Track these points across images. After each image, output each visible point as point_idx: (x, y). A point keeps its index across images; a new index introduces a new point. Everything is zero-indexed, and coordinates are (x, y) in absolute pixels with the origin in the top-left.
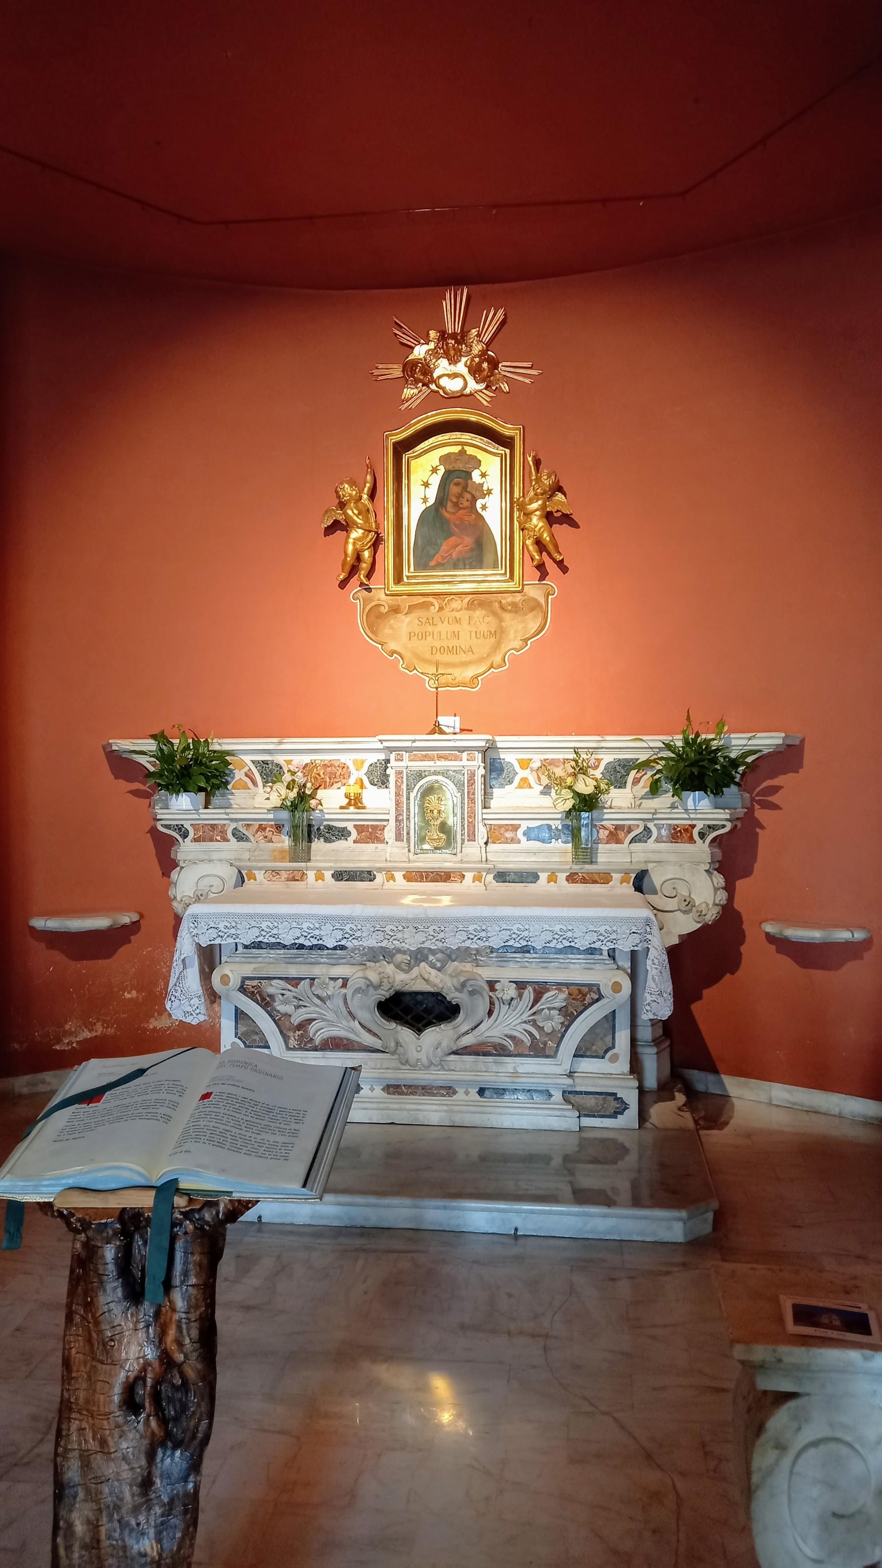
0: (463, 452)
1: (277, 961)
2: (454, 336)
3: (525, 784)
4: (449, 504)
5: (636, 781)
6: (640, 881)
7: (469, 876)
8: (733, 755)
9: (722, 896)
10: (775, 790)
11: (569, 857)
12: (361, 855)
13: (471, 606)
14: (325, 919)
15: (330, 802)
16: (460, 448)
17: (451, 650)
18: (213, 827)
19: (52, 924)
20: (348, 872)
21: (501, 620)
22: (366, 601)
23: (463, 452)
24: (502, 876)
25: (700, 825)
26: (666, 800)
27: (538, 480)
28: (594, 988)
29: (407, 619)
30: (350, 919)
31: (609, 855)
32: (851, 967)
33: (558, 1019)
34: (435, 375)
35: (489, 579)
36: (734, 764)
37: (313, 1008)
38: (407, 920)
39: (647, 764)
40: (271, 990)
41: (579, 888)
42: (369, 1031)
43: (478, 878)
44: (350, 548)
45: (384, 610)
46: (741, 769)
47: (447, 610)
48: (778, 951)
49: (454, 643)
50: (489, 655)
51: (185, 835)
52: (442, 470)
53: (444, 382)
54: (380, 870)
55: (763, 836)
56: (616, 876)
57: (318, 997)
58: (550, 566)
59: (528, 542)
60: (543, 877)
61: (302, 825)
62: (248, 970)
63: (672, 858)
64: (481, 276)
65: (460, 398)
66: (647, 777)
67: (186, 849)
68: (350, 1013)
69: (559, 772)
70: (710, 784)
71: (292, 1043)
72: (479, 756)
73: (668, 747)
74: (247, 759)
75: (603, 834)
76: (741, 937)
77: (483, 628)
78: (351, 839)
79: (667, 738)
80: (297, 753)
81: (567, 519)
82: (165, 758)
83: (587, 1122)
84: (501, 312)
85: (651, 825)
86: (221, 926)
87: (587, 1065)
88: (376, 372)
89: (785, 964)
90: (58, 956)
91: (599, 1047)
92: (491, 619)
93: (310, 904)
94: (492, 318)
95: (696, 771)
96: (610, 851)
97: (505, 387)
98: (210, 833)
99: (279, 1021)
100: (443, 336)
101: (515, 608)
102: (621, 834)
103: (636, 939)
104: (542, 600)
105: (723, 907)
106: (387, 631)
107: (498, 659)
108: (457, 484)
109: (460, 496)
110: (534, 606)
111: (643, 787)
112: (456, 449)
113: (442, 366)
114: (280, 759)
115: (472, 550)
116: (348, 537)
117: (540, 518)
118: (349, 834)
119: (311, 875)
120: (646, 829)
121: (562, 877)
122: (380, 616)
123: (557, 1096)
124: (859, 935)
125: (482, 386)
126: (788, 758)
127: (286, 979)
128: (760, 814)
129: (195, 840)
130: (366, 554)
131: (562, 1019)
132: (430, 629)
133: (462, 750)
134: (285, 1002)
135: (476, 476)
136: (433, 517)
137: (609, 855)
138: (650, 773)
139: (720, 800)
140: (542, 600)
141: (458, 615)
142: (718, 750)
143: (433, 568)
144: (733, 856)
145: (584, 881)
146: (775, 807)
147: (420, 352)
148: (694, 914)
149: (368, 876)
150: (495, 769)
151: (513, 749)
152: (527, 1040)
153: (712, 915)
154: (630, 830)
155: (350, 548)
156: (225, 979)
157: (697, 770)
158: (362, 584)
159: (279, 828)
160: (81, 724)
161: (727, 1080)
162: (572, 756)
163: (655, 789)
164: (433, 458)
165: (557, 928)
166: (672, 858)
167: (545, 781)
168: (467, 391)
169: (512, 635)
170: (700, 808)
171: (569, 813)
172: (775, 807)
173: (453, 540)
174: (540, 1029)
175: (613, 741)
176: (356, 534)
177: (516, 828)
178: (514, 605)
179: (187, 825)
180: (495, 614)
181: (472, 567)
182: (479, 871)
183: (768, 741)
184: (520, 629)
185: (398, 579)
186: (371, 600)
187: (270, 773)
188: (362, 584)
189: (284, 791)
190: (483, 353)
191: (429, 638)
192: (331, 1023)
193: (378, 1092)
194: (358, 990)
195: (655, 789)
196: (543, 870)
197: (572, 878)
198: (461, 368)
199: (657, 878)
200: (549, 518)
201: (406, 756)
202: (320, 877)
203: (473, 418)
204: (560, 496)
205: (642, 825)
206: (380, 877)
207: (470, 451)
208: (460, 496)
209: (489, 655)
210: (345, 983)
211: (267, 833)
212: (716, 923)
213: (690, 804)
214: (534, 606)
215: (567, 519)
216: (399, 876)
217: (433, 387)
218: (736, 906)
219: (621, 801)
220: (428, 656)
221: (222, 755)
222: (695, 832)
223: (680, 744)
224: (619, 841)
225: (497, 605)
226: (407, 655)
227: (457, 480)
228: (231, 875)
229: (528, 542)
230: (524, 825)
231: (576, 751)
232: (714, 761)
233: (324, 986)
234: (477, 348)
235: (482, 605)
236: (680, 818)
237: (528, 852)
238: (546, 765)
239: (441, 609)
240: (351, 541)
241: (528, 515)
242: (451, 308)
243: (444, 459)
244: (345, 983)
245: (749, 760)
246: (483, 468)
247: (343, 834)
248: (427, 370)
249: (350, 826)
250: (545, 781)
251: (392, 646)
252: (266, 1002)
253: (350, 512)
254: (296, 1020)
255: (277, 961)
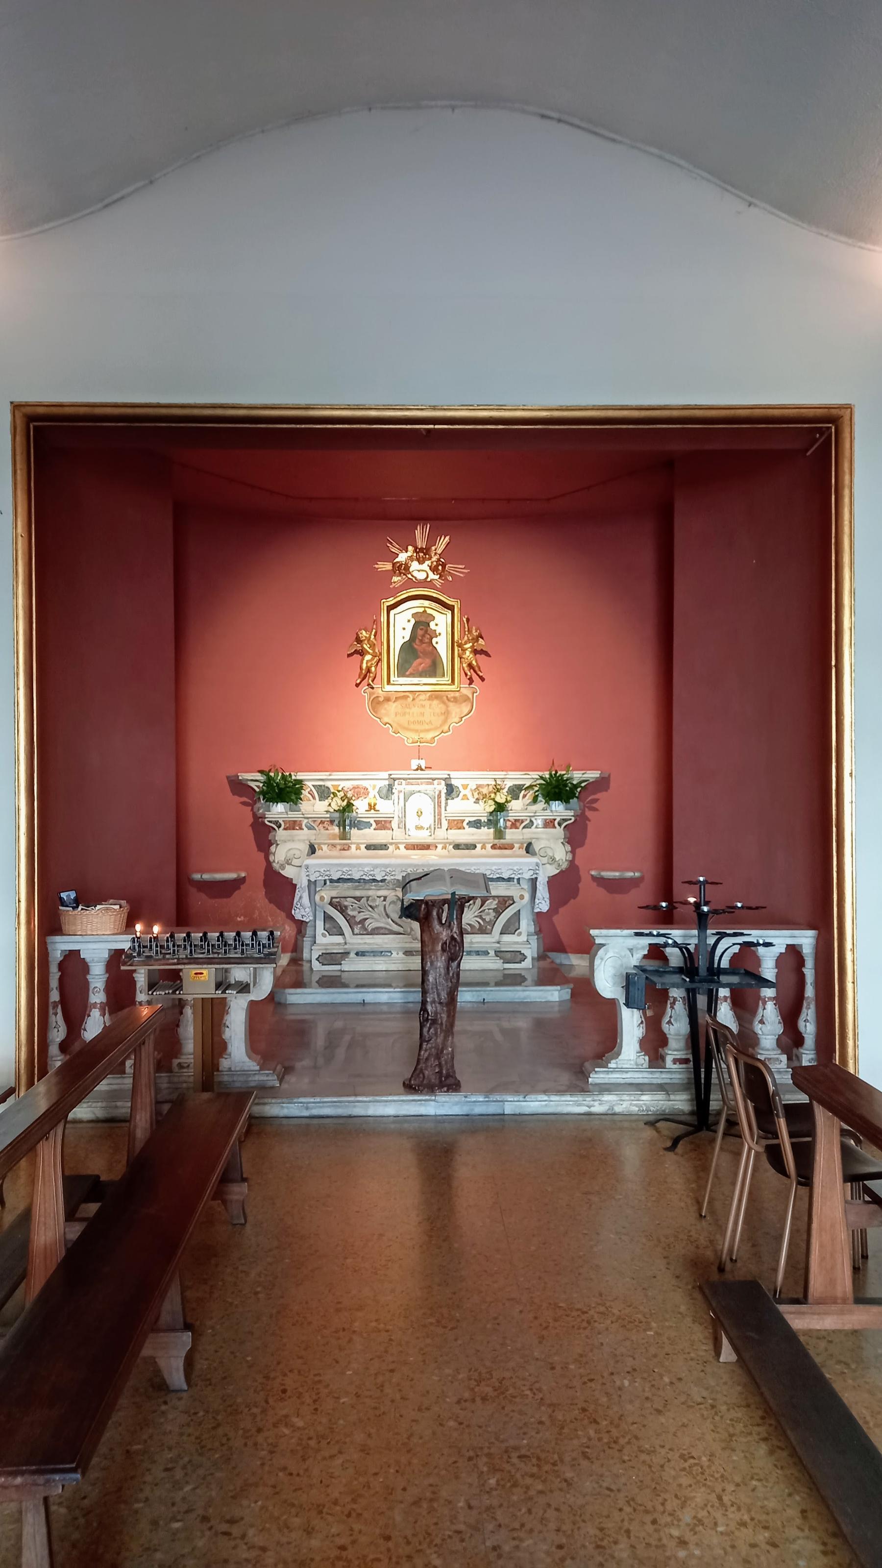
0: (425, 611)
1: (348, 888)
2: (421, 550)
3: (465, 797)
4: (417, 641)
5: (524, 796)
6: (529, 849)
7: (440, 846)
8: (575, 782)
9: (570, 857)
10: (596, 800)
11: (492, 836)
12: (381, 836)
13: (430, 698)
14: (376, 866)
15: (360, 806)
16: (422, 609)
17: (419, 722)
18: (295, 822)
19: (206, 877)
20: (374, 845)
21: (447, 707)
22: (371, 694)
23: (425, 611)
24: (457, 847)
25: (558, 819)
26: (541, 805)
27: (470, 631)
28: (511, 898)
29: (395, 705)
30: (387, 866)
31: (511, 835)
32: (634, 892)
33: (493, 914)
34: (411, 570)
35: (440, 683)
36: (575, 786)
37: (368, 913)
38: (418, 865)
39: (531, 787)
40: (346, 903)
41: (498, 852)
42: (396, 924)
43: (444, 848)
44: (364, 666)
45: (381, 699)
46: (579, 790)
47: (417, 700)
48: (598, 885)
49: (421, 719)
50: (441, 726)
51: (279, 827)
52: (413, 621)
53: (415, 574)
54: (392, 844)
55: (590, 827)
56: (517, 846)
57: (371, 906)
58: (475, 677)
59: (464, 665)
60: (479, 846)
61: (345, 819)
62: (334, 893)
63: (544, 836)
64: (439, 517)
65: (425, 583)
66: (531, 794)
67: (281, 834)
68: (387, 915)
69: (485, 791)
70: (565, 797)
71: (356, 931)
72: (443, 782)
73: (542, 778)
74: (310, 784)
75: (509, 824)
76: (579, 879)
77: (438, 711)
78: (372, 828)
79: (541, 773)
80: (342, 781)
81: (482, 652)
82: (269, 782)
83: (507, 966)
84: (447, 538)
85: (533, 819)
86: (322, 870)
87: (507, 938)
88: (376, 566)
89: (601, 892)
90: (203, 896)
91: (512, 929)
92: (442, 705)
93: (357, 860)
94: (443, 542)
95: (557, 790)
96: (513, 833)
97: (450, 579)
98: (293, 825)
99: (351, 921)
100: (416, 550)
101: (455, 700)
102: (518, 824)
103: (531, 872)
104: (471, 696)
105: (570, 861)
106: (383, 711)
107: (446, 728)
108: (422, 629)
109: (423, 636)
110: (466, 699)
111: (529, 798)
112: (421, 610)
113: (415, 566)
114: (329, 784)
115: (430, 666)
116: (363, 659)
117: (471, 652)
118: (371, 825)
119: (353, 847)
120: (531, 821)
121: (489, 846)
122: (379, 703)
123: (492, 953)
124: (637, 874)
125: (437, 577)
126: (602, 784)
127: (354, 898)
128: (588, 813)
129: (285, 829)
130: (373, 669)
131: (494, 914)
132: (407, 710)
133: (434, 779)
134: (353, 910)
135: (432, 625)
136: (408, 648)
137: (511, 835)
138: (531, 792)
139: (568, 806)
140: (471, 696)
141: (424, 703)
142: (567, 780)
143: (408, 676)
144: (575, 834)
145: (500, 848)
146: (596, 810)
147: (402, 557)
148: (555, 865)
149: (384, 847)
150: (451, 790)
151: (459, 778)
152: (477, 925)
153: (565, 866)
154: (522, 822)
155: (364, 666)
156: (322, 898)
157: (556, 790)
158: (369, 685)
159: (332, 822)
160: (218, 761)
161: (572, 956)
162: (494, 783)
163: (535, 800)
164: (408, 615)
165: (493, 868)
166: (544, 836)
167: (476, 796)
168: (429, 580)
169: (453, 715)
170: (558, 809)
171: (491, 813)
172: (596, 810)
173: (419, 660)
174: (484, 920)
175: (512, 774)
176: (368, 657)
177: (463, 821)
178: (455, 698)
179: (281, 821)
180: (444, 703)
181: (430, 676)
182: (445, 844)
183: (593, 775)
184: (458, 711)
185: (389, 682)
186: (374, 693)
187: (324, 793)
188: (369, 685)
189: (339, 802)
190: (439, 560)
191: (407, 716)
192: (377, 920)
193: (401, 955)
194: (393, 902)
195: (535, 800)
196: (479, 843)
197: (494, 847)
198: (425, 566)
199: (536, 847)
200: (475, 652)
201: (404, 782)
202: (358, 848)
203: (435, 595)
204: (481, 641)
205: (528, 819)
206: (391, 848)
207: (429, 611)
208: (423, 636)
209: (441, 726)
210: (385, 898)
211: (325, 825)
212: (567, 869)
213: (553, 808)
214: (466, 699)
215: (482, 652)
216: (402, 847)
217: (409, 576)
218: (577, 862)
219: (516, 807)
220: (406, 725)
221: (300, 782)
222: (556, 823)
223: (548, 776)
224: (517, 828)
225: (445, 698)
226: (394, 725)
227: (422, 625)
228: (306, 848)
229: (464, 665)
230: (467, 820)
231: (495, 780)
232: (566, 785)
233: (374, 900)
234: (434, 559)
235: (437, 697)
236: (549, 816)
237: (469, 834)
238: (479, 787)
239: (414, 699)
240: (365, 662)
241: (464, 650)
242: (421, 535)
243: (414, 615)
244: (385, 898)
245: (583, 785)
246: (436, 621)
247: (369, 825)
248: (407, 568)
249: (372, 821)
250: (476, 796)
251: (386, 720)
252: (342, 910)
253: (365, 646)
254: (358, 919)
255: (348, 888)
